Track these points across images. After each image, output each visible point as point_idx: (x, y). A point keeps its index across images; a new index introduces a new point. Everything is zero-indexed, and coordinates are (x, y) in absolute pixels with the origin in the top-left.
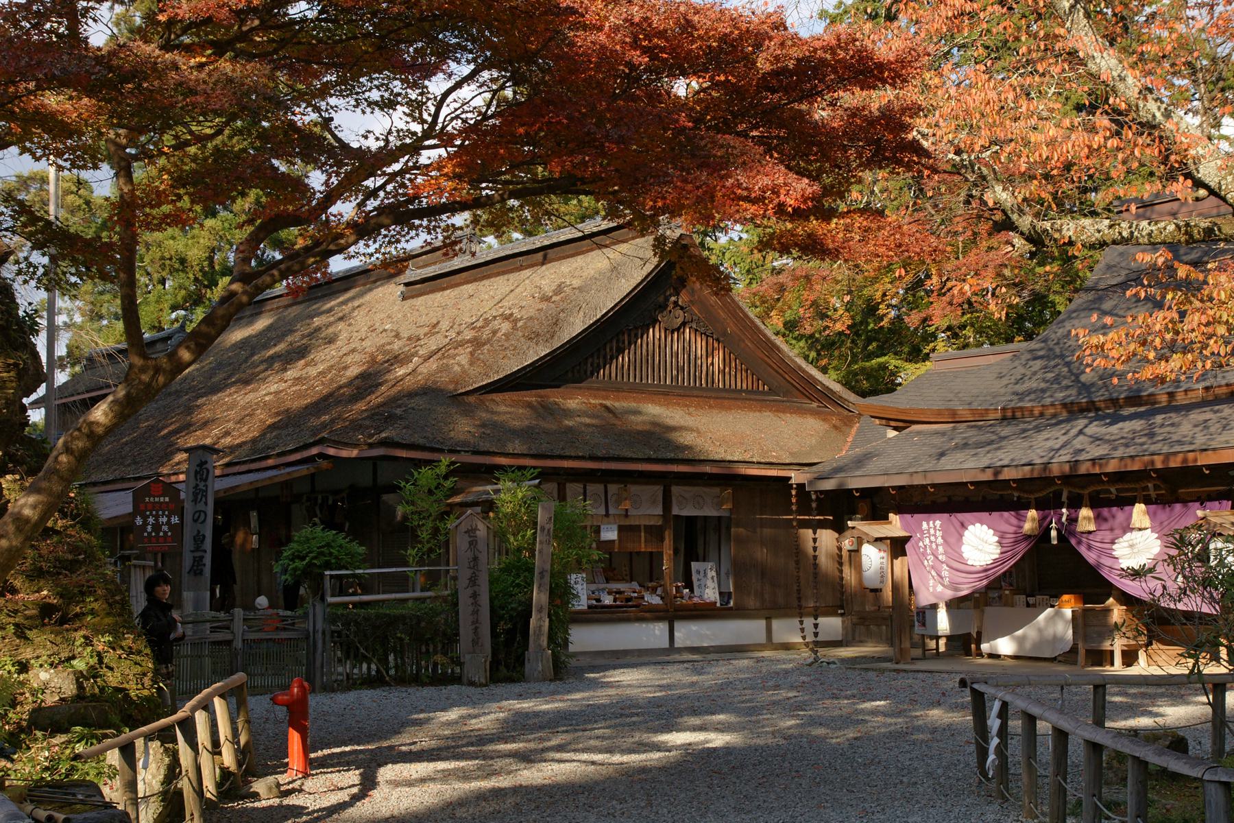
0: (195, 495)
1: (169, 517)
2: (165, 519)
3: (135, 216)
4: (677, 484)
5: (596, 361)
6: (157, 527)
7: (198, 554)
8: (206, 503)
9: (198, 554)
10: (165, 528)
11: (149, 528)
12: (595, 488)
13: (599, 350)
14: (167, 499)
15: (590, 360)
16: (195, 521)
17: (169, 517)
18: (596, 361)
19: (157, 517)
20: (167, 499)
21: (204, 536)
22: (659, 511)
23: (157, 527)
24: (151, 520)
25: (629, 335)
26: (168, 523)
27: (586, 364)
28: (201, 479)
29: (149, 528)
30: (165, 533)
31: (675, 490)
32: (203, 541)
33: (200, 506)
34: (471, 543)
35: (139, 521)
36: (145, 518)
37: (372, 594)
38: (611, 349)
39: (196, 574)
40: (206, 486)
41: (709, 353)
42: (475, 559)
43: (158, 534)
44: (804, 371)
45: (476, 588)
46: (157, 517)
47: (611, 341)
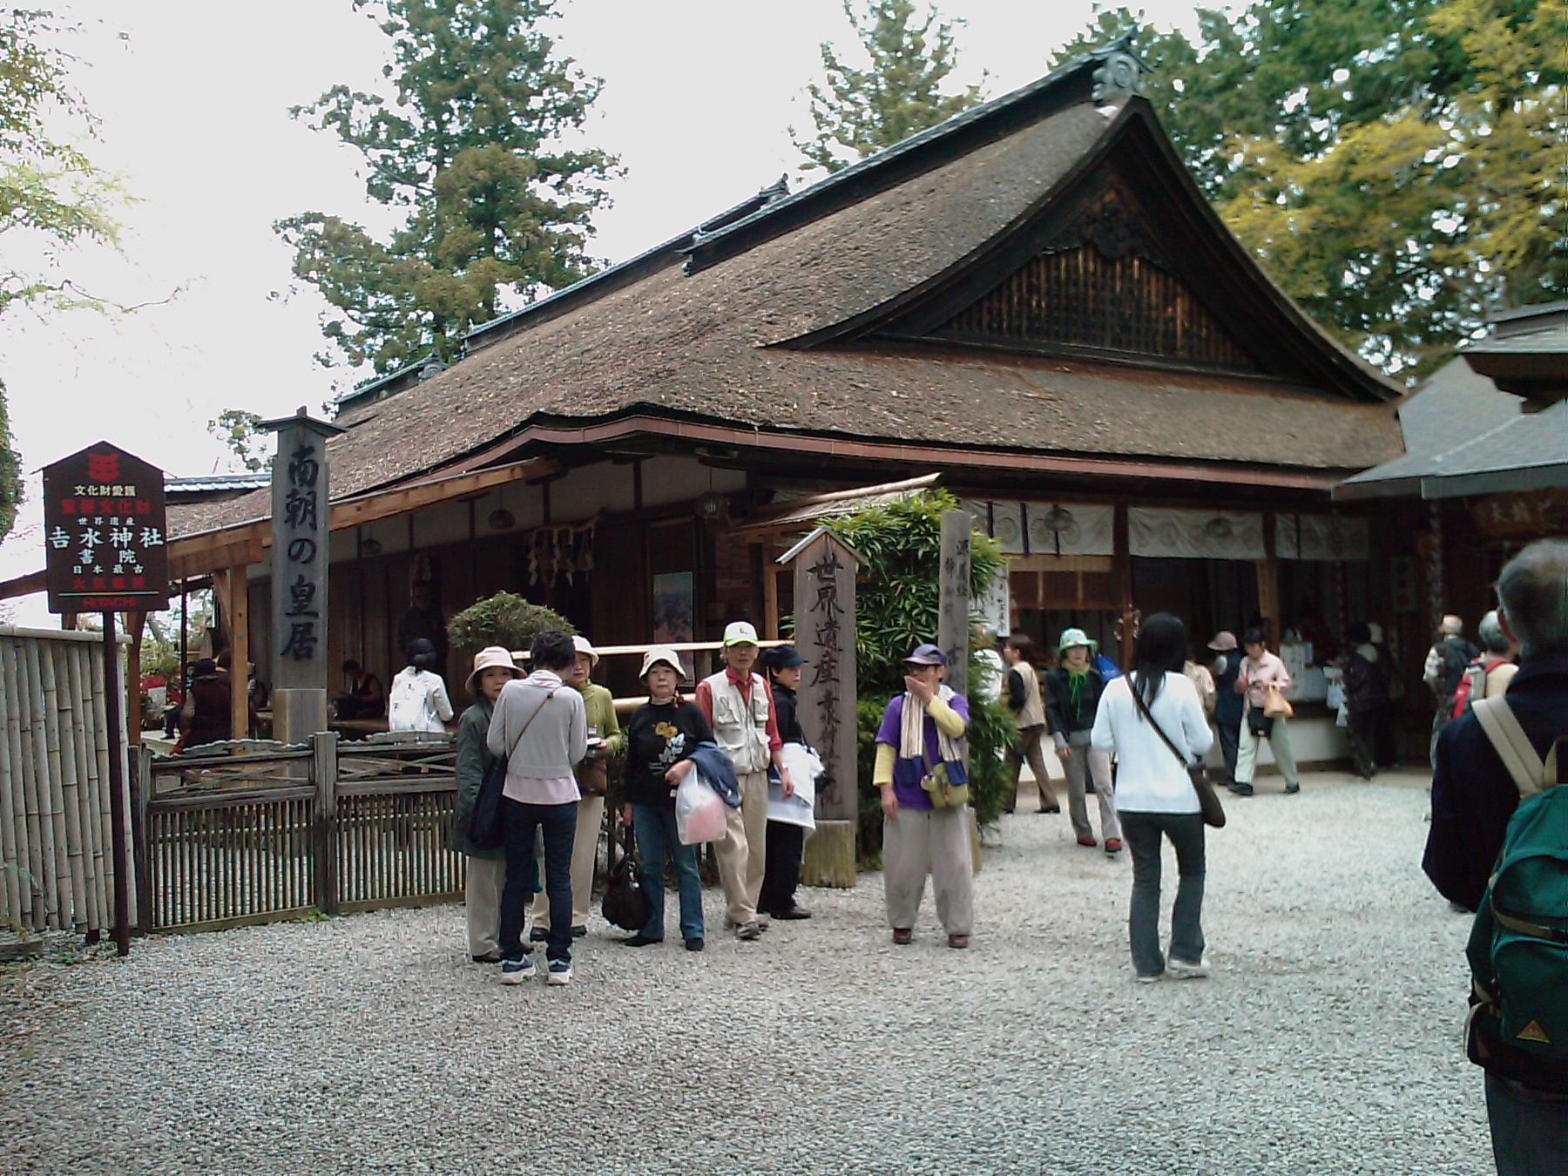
0: (292, 510)
2: (126, 537)
3: (427, 310)
4: (1137, 504)
5: (996, 305)
6: (106, 553)
7: (303, 620)
8: (314, 526)
9: (303, 620)
10: (127, 556)
12: (1007, 509)
13: (999, 288)
14: (130, 491)
15: (986, 304)
16: (293, 558)
17: (136, 531)
18: (996, 305)
19: (105, 531)
20: (130, 491)
21: (312, 588)
22: (1108, 549)
23: (106, 553)
24: (91, 537)
25: (1048, 267)
26: (135, 544)
27: (980, 311)
28: (303, 482)
30: (126, 565)
31: (1137, 514)
32: (309, 596)
33: (303, 532)
34: (822, 593)
37: (695, 651)
38: (1020, 289)
39: (298, 657)
40: (313, 494)
41: (1169, 300)
42: (831, 625)
43: (108, 568)
44: (1313, 332)
45: (831, 685)
46: (105, 531)
47: (1018, 273)
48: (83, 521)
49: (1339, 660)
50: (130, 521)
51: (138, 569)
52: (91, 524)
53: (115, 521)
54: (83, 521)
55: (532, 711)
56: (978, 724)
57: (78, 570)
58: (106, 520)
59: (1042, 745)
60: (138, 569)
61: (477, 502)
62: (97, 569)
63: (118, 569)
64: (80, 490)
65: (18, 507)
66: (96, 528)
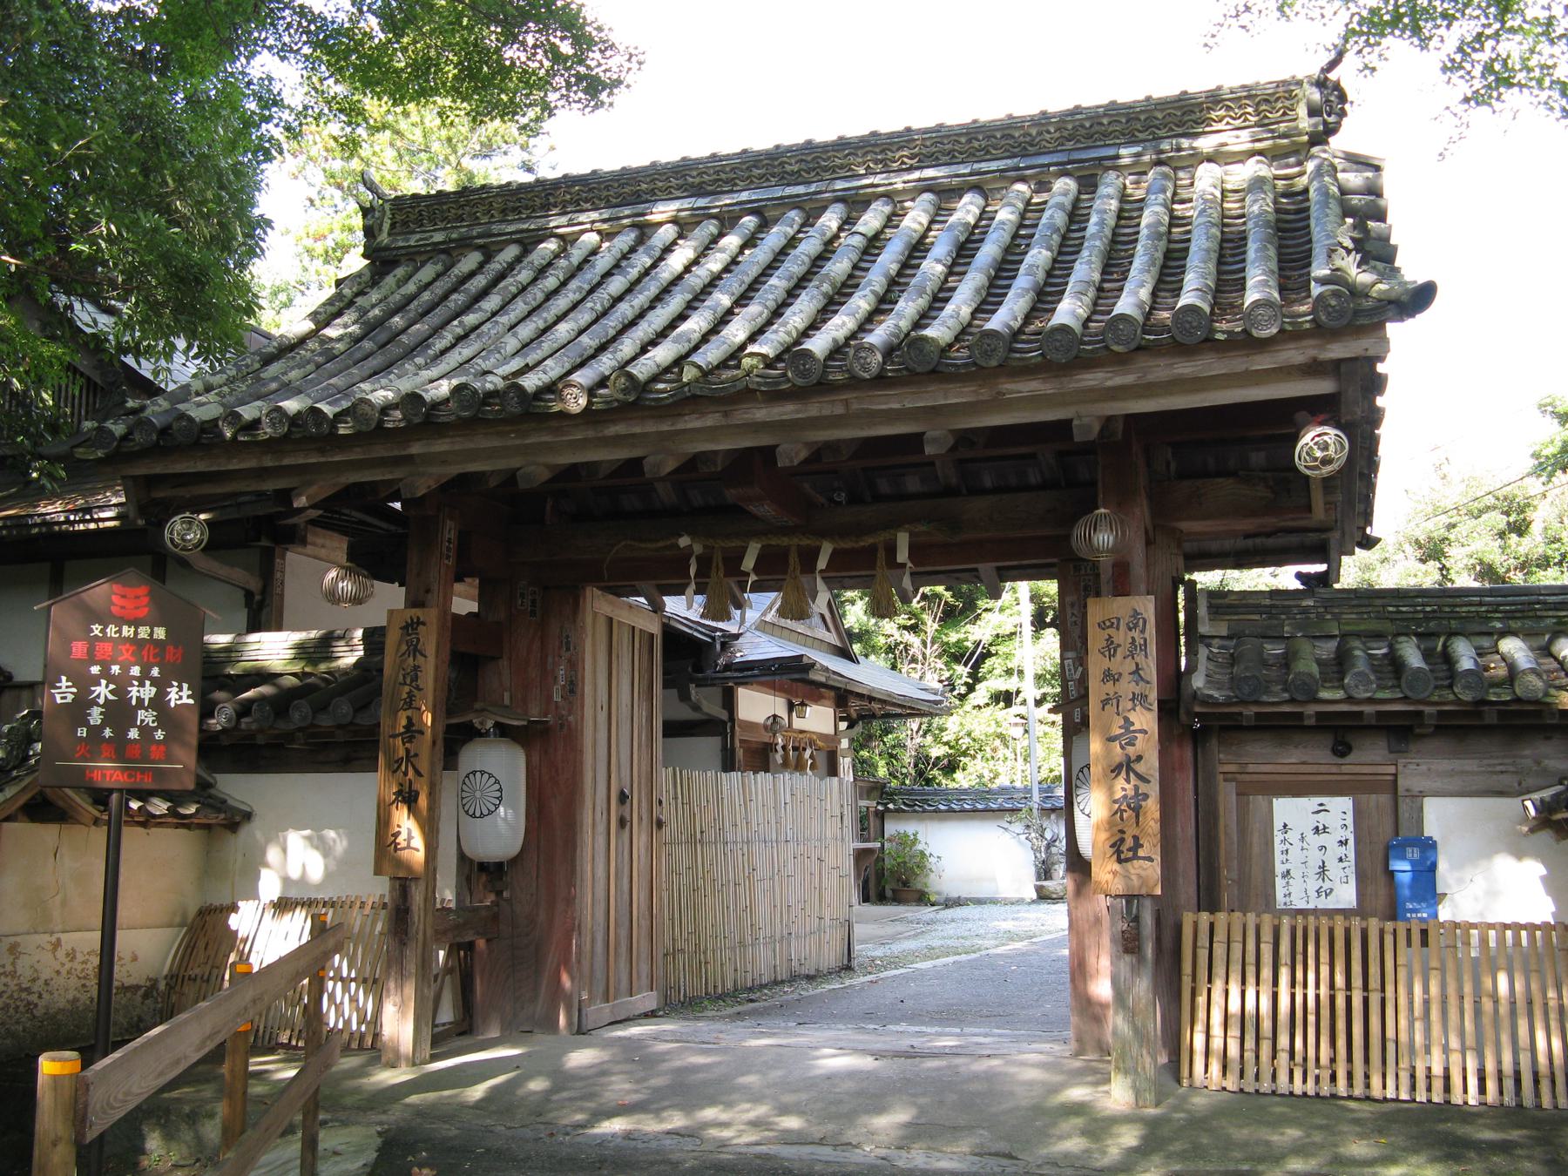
1: (161, 685)
2: (148, 692)
10: (146, 717)
11: (96, 716)
17: (161, 685)
26: (159, 703)
29: (96, 716)
30: (145, 731)
43: (121, 732)
48: (95, 670)
49: (145, 1129)
50: (155, 672)
51: (159, 735)
52: (106, 673)
53: (135, 671)
54: (95, 670)
55: (763, 963)
56: (314, 910)
57: (82, 732)
58: (125, 669)
59: (270, 959)
60: (159, 735)
61: (1385, 799)
62: (108, 733)
63: (133, 734)
64: (160, 633)
65: (920, 847)
66: (111, 679)
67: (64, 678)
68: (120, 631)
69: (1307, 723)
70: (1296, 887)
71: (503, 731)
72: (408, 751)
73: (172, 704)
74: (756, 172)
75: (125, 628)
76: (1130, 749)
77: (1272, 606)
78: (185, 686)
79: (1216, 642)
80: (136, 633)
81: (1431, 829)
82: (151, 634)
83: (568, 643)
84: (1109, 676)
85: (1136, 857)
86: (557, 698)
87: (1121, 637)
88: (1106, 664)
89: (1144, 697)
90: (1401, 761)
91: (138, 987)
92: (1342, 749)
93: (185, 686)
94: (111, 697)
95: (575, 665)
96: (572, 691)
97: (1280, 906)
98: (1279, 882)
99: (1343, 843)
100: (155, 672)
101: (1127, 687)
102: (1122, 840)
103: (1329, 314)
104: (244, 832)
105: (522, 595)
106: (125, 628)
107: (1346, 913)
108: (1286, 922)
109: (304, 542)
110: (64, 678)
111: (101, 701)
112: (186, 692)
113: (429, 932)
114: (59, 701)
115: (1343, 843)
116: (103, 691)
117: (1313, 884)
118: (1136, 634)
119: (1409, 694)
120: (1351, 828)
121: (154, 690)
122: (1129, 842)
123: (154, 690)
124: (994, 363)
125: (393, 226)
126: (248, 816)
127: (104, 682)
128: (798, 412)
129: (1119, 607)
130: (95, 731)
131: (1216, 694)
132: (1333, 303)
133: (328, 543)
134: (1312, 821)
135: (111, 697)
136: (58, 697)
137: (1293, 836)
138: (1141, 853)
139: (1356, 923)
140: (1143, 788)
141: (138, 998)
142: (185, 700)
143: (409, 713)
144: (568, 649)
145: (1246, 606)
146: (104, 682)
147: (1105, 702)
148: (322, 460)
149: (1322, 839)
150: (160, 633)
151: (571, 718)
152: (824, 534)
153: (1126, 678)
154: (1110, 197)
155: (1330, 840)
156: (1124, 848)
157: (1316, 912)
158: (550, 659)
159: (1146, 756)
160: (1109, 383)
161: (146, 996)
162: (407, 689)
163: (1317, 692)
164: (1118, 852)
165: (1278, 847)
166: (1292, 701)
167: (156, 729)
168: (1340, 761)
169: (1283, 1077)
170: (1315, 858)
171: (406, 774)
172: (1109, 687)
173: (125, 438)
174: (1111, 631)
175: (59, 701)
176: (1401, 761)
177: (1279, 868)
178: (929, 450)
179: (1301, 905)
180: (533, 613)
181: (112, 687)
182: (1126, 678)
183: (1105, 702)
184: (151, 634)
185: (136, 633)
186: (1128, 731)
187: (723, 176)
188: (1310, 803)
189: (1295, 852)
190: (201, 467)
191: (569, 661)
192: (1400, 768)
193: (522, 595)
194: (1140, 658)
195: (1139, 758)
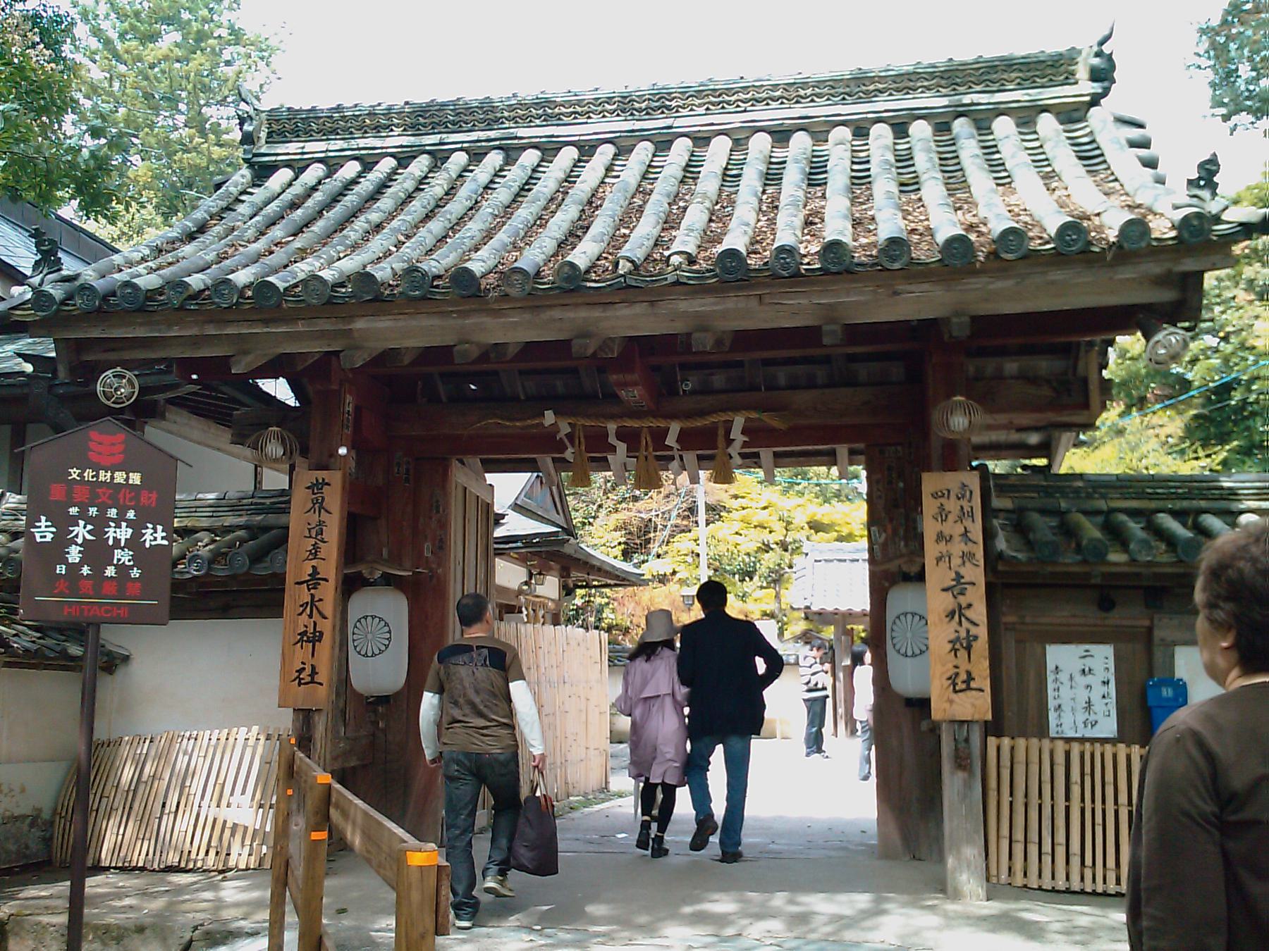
1: (137, 527)
2: (124, 533)
6: (98, 552)
11: (74, 554)
14: (135, 478)
17: (137, 527)
23: (98, 552)
24: (81, 531)
26: (134, 542)
29: (74, 554)
35: (44, 531)
36: (63, 524)
43: (98, 570)
46: (100, 525)
48: (74, 511)
50: (131, 514)
51: (135, 573)
52: (83, 515)
53: (113, 513)
54: (74, 511)
57: (61, 569)
62: (86, 570)
63: (110, 571)
66: (89, 520)
67: (43, 518)
68: (97, 476)
69: (1093, 581)
70: (1067, 719)
71: (388, 581)
72: (313, 596)
73: (147, 545)
74: (608, 107)
75: (102, 473)
76: (961, 598)
77: (1048, 487)
78: (160, 528)
79: (1002, 515)
80: (112, 478)
81: (1181, 672)
82: (127, 479)
83: (438, 507)
84: (940, 537)
85: (969, 688)
86: (427, 554)
87: (952, 505)
88: (939, 527)
89: (972, 555)
90: (1156, 617)
91: (25, 817)
92: (1106, 604)
93: (160, 528)
94: (89, 537)
95: (444, 525)
96: (441, 548)
97: (1052, 734)
98: (1052, 716)
99: (1106, 683)
100: (131, 514)
101: (958, 548)
102: (957, 674)
103: (1191, 233)
104: (120, 673)
105: (399, 465)
106: (102, 473)
107: (1103, 741)
108: (1060, 747)
109: (163, 417)
110: (43, 518)
111: (80, 541)
112: (160, 534)
113: (328, 757)
114: (39, 540)
115: (1106, 683)
116: (81, 531)
117: (1081, 717)
118: (964, 503)
119: (1184, 558)
120: (1112, 669)
121: (130, 531)
122: (963, 676)
123: (130, 531)
124: (897, 266)
125: (270, 135)
126: (126, 659)
127: (82, 523)
128: (714, 304)
129: (952, 480)
130: (74, 568)
131: (1020, 556)
132: (1195, 223)
133: (178, 419)
134: (1080, 664)
135: (89, 537)
136: (38, 536)
137: (1063, 677)
138: (973, 685)
139: (1122, 747)
140: (974, 631)
141: (25, 827)
142: (159, 541)
143: (314, 563)
144: (438, 512)
145: (1029, 486)
146: (82, 523)
147: (939, 560)
148: (266, 330)
149: (1089, 679)
150: (135, 478)
151: (440, 571)
152: (673, 416)
153: (957, 539)
154: (356, 231)
155: (1094, 680)
156: (959, 681)
157: (1082, 740)
158: (421, 520)
159: (975, 604)
160: (991, 287)
161: (32, 825)
162: (313, 541)
163: (1106, 555)
164: (955, 685)
165: (1050, 686)
166: (1085, 562)
167: (131, 567)
168: (1104, 615)
169: (1075, 877)
170: (1082, 695)
171: (310, 616)
172: (942, 547)
173: (63, 303)
174: (943, 500)
175: (39, 540)
176: (1156, 617)
177: (1052, 704)
178: (826, 340)
179: (1071, 734)
180: (407, 480)
181: (89, 527)
182: (957, 539)
183: (939, 560)
184: (127, 479)
185: (112, 478)
186: (959, 583)
187: (579, 109)
188: (1079, 649)
189: (1065, 692)
190: (141, 332)
191: (439, 521)
192: (1156, 622)
193: (399, 465)
194: (968, 523)
195: (970, 606)
